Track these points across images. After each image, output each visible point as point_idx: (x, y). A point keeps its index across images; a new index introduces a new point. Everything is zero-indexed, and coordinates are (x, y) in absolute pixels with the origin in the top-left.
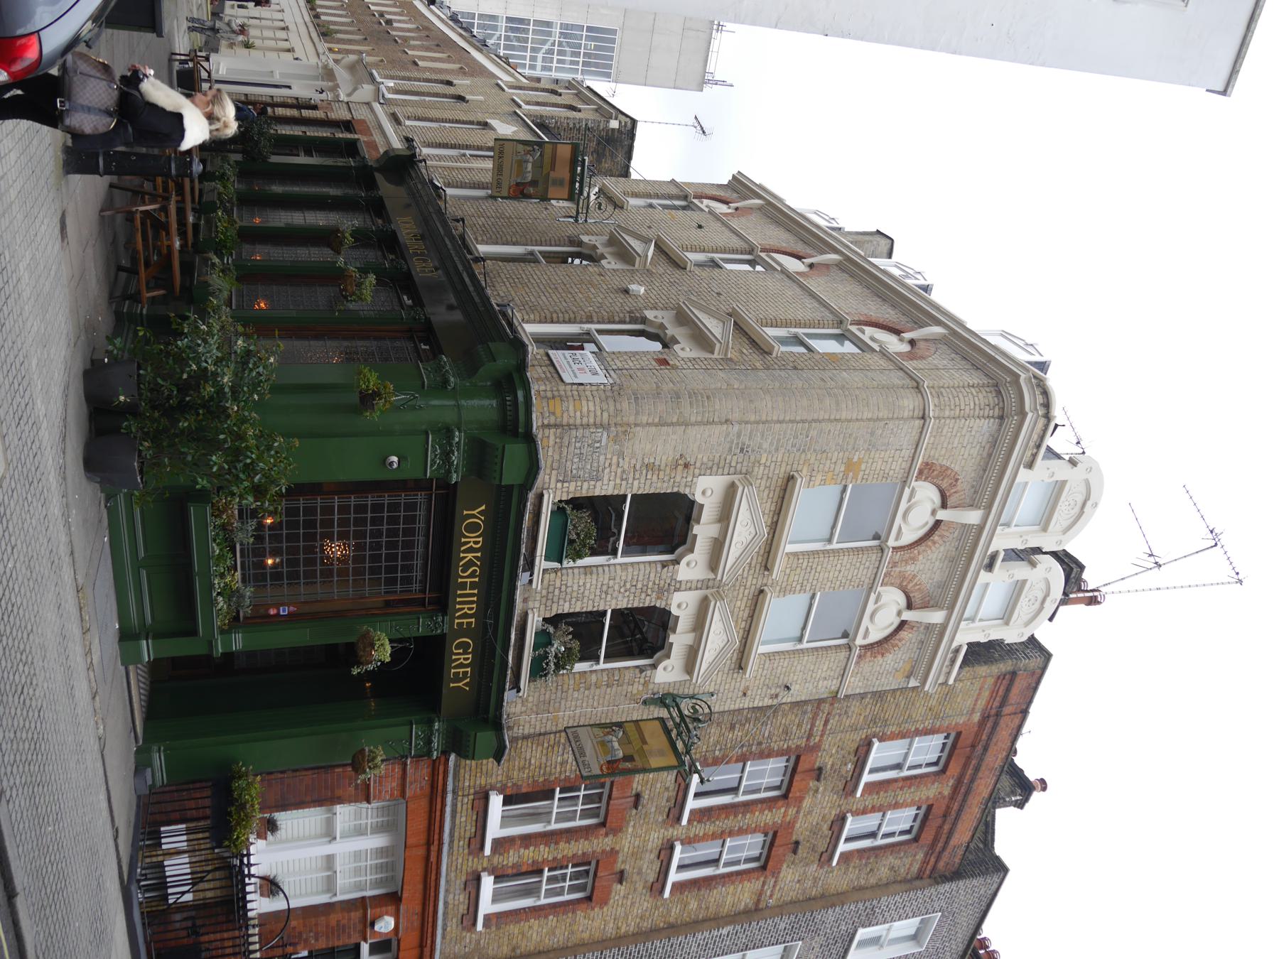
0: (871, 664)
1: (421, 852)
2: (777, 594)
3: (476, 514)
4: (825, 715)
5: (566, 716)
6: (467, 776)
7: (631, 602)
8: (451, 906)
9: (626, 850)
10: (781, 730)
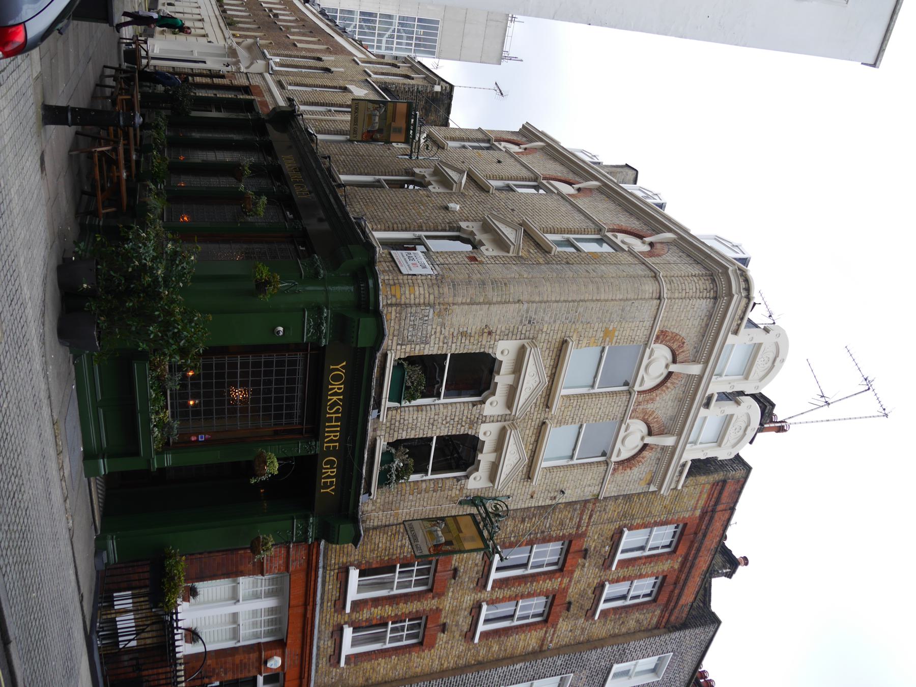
0: (622, 475)
1: (300, 610)
2: (555, 425)
4: (589, 512)
6: (333, 556)
7: (450, 431)
9: (447, 608)
10: (558, 522)
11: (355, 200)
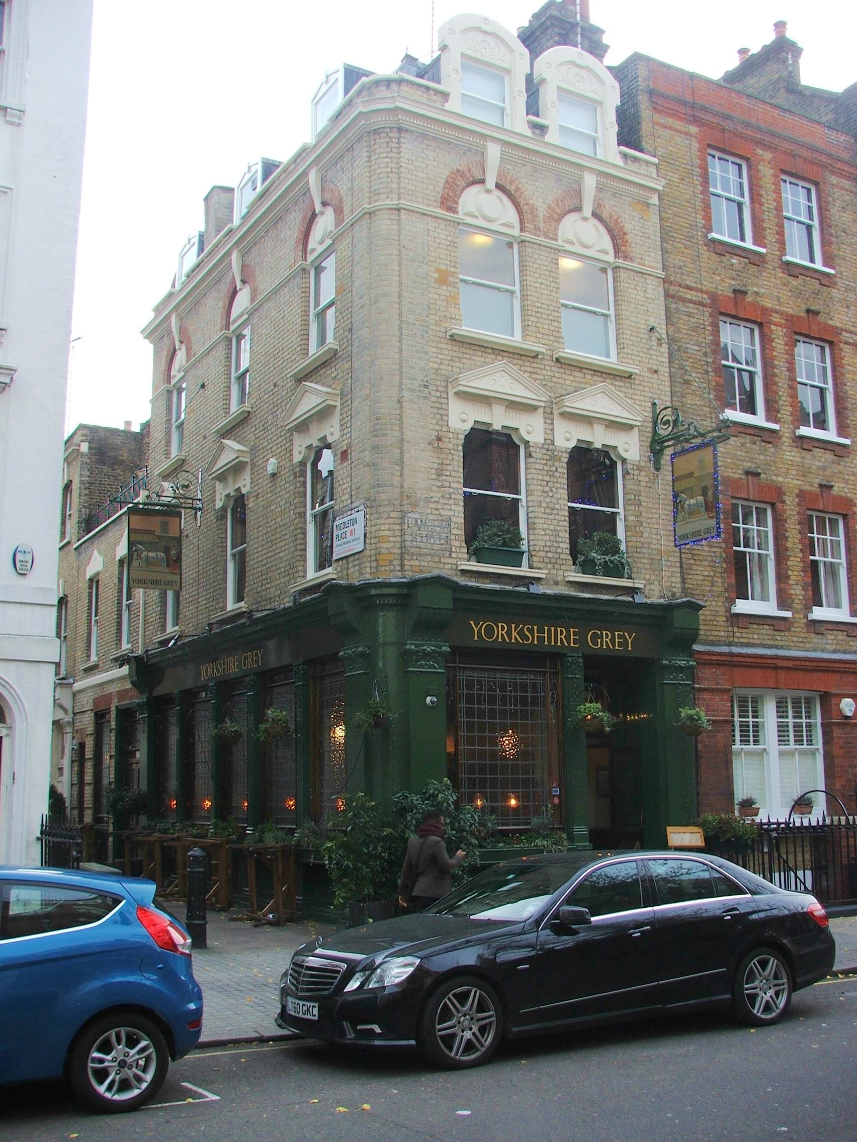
0: (633, 245)
1: (782, 674)
2: (561, 345)
3: (478, 629)
4: (681, 289)
5: (666, 543)
6: (716, 633)
7: (562, 486)
8: (838, 647)
9: (799, 483)
10: (693, 334)
11: (264, 593)
